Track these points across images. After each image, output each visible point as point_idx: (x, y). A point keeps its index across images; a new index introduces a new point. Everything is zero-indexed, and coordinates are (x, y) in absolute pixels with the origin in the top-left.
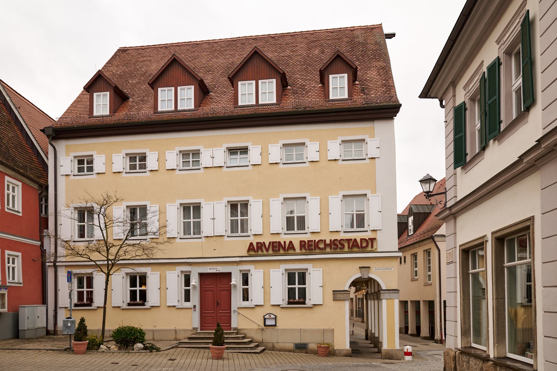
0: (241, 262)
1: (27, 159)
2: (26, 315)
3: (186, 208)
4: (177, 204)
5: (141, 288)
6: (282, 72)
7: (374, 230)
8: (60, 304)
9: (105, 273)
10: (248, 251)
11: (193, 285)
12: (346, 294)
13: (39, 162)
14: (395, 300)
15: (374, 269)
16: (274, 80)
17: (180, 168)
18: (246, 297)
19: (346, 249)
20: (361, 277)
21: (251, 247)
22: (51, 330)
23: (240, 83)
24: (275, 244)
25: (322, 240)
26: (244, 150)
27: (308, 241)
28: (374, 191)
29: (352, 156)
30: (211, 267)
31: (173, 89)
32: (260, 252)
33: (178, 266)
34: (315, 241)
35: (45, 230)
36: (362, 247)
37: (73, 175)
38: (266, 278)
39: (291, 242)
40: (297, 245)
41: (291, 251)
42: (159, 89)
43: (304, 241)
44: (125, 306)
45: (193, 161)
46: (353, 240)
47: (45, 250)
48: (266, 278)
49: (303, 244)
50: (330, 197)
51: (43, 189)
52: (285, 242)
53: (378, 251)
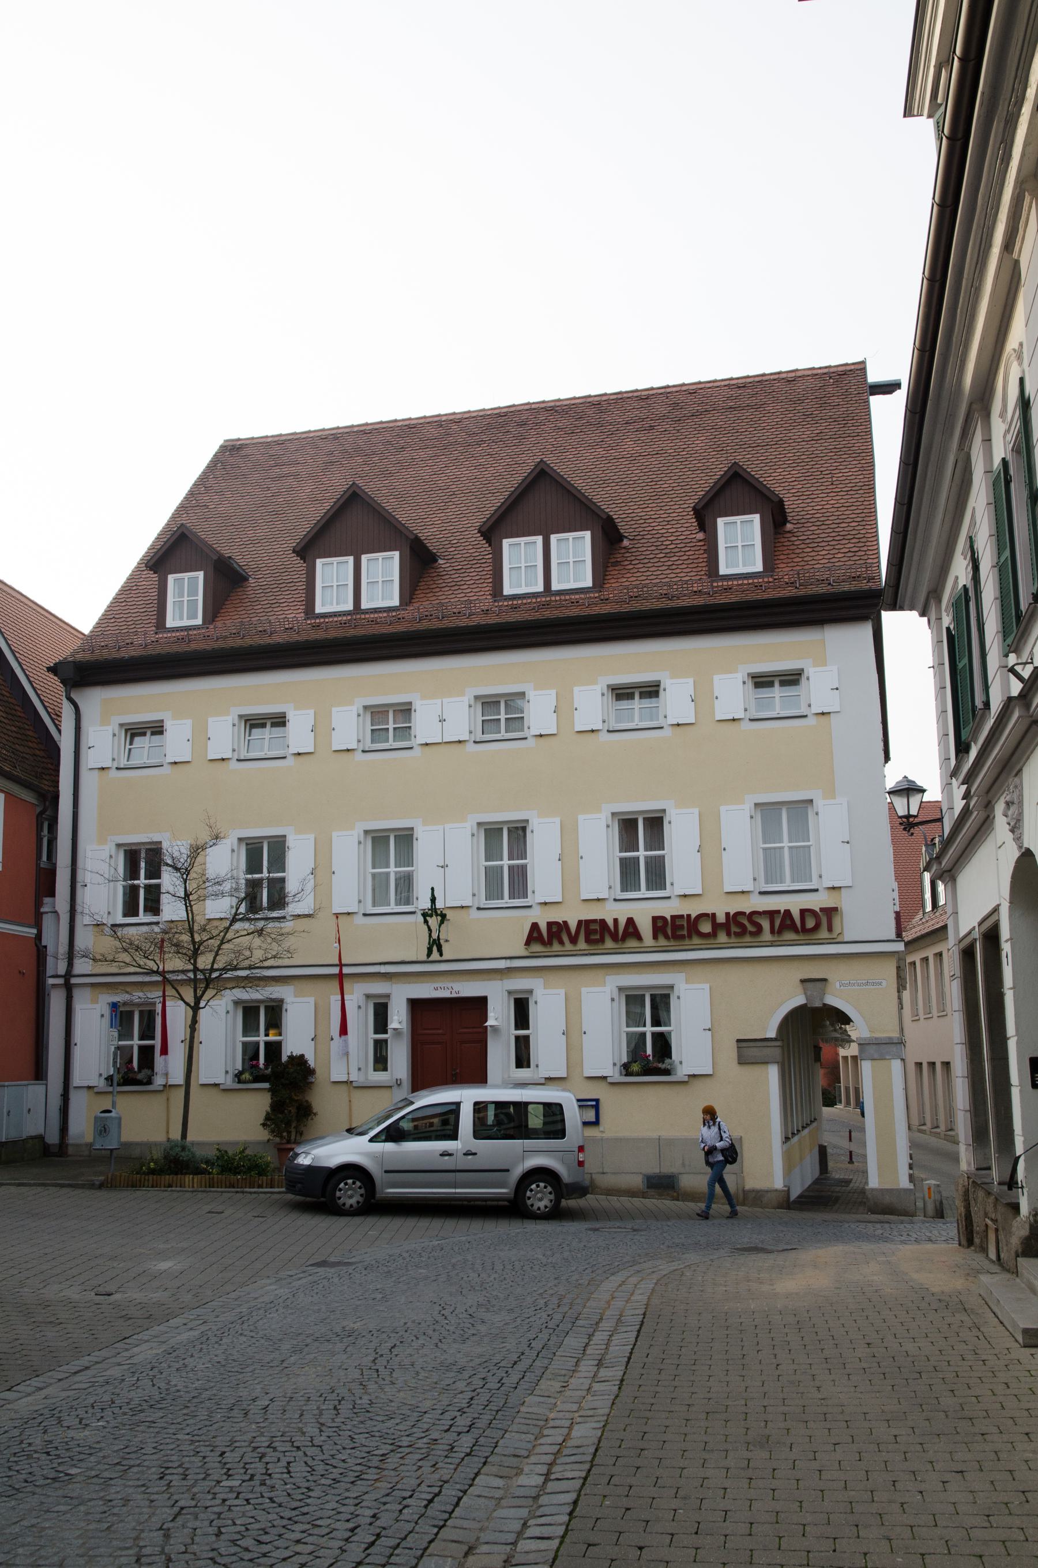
0: (509, 970)
1: (15, 735)
2: (5, 1105)
3: (378, 840)
4: (357, 833)
5: (641, 1029)
6: (604, 517)
7: (834, 888)
8: (77, 1080)
9: (187, 1004)
10: (528, 943)
11: (394, 1029)
12: (769, 1049)
13: (36, 736)
14: (893, 1061)
15: (838, 985)
16: (756, 518)
17: (239, 755)
18: (523, 1059)
19: (766, 935)
20: (806, 1004)
21: (535, 935)
22: (54, 1145)
23: (720, 521)
24: (593, 927)
25: (706, 915)
26: (651, 691)
27: (673, 917)
28: (830, 793)
29: (262, 750)
30: (436, 985)
31: (539, 539)
32: (556, 947)
33: (358, 982)
34: (689, 916)
35: (47, 900)
36: (805, 930)
37: (238, 760)
38: (572, 1009)
39: (630, 921)
40: (645, 927)
41: (632, 943)
42: (506, 543)
43: (663, 918)
44: (228, 1081)
45: (395, 729)
46: (782, 911)
47: (45, 947)
48: (572, 1009)
49: (661, 926)
50: (723, 809)
51: (47, 803)
52: (616, 921)
53: (845, 940)
